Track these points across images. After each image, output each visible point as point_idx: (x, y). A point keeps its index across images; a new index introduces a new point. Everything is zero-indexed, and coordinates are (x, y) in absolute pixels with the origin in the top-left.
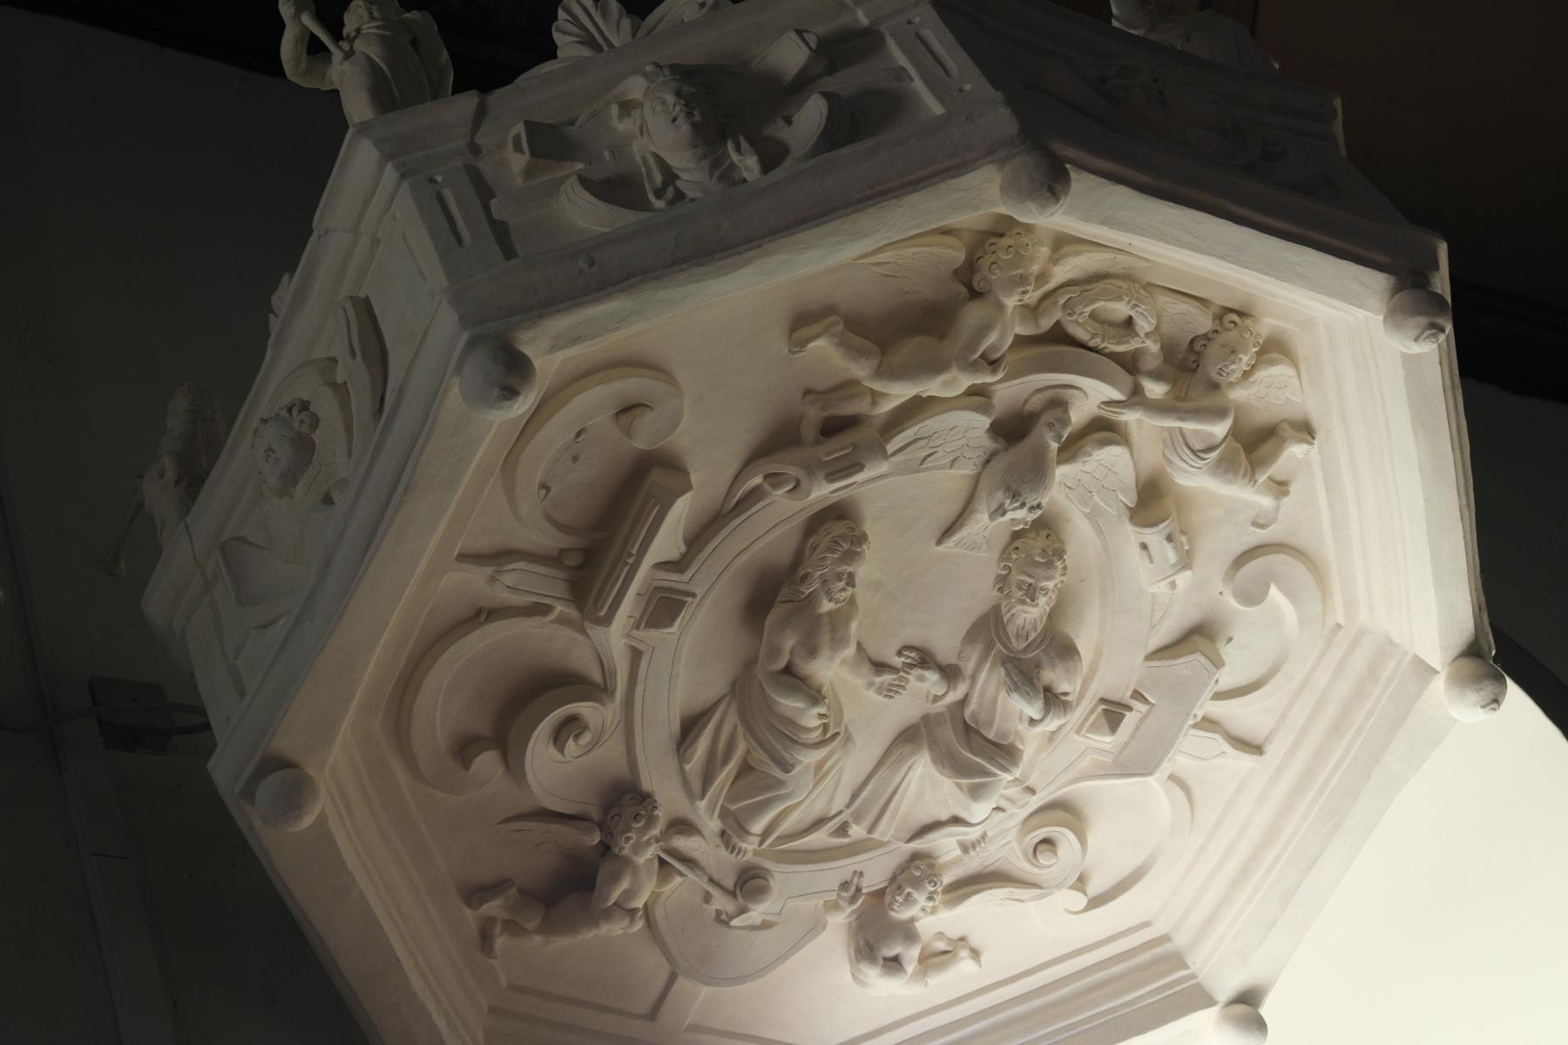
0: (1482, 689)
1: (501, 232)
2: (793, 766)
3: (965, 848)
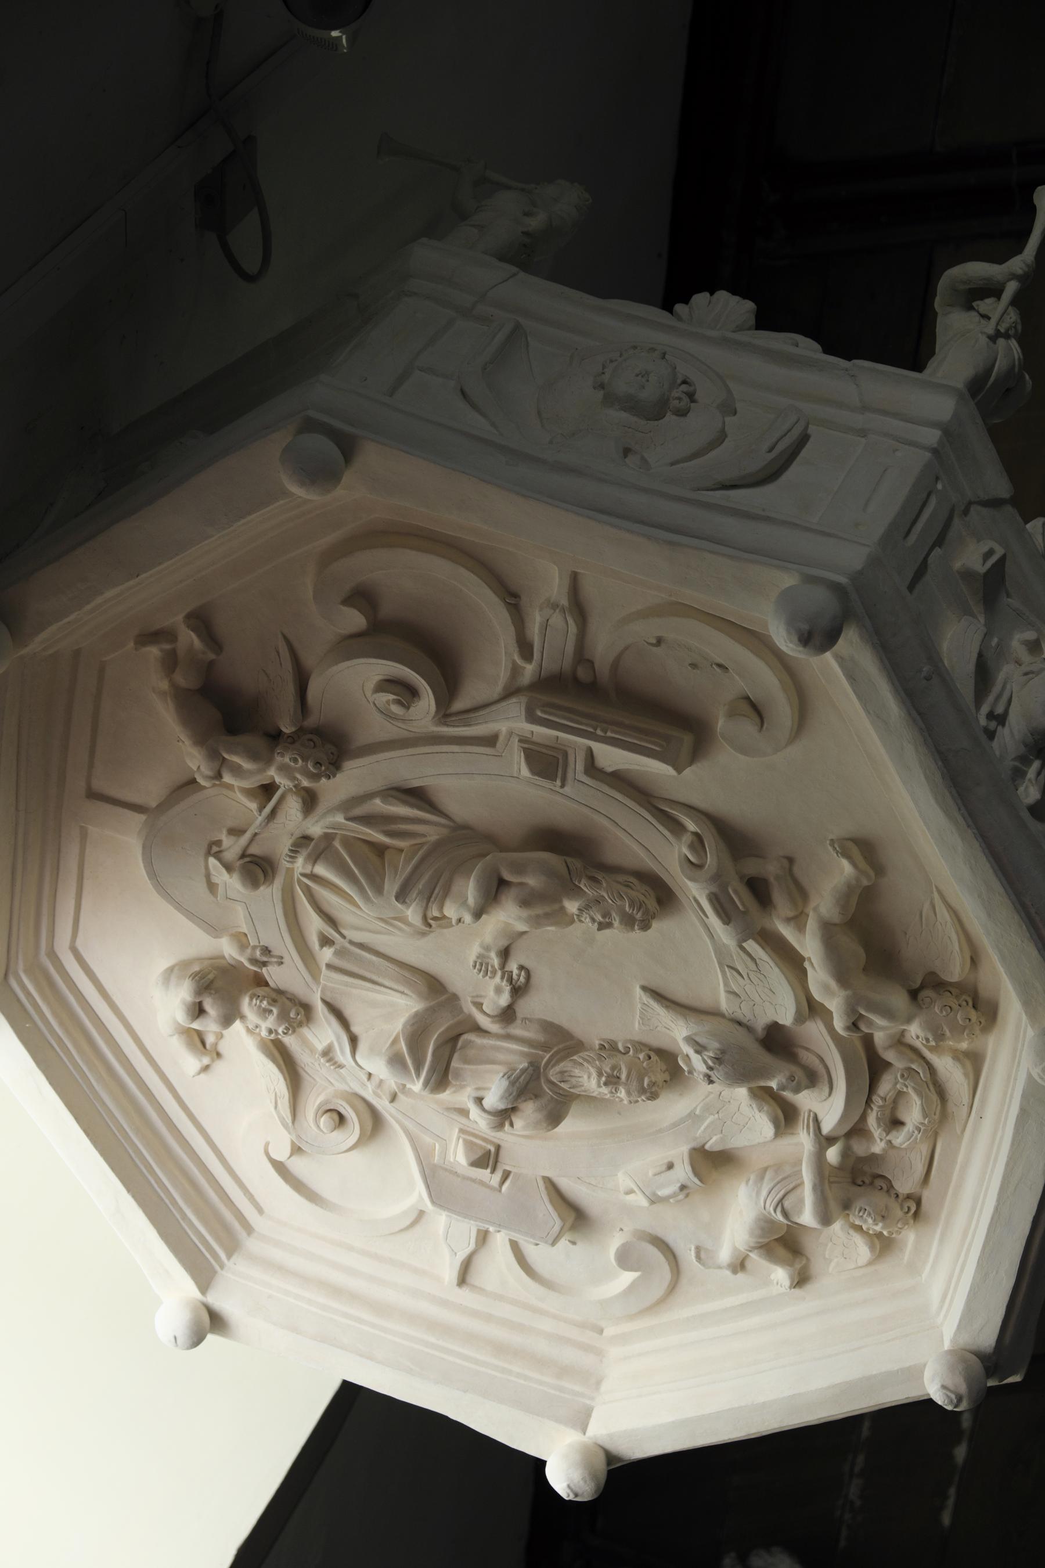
0: (585, 1482)
1: (922, 570)
2: (404, 902)
3: (327, 1053)
